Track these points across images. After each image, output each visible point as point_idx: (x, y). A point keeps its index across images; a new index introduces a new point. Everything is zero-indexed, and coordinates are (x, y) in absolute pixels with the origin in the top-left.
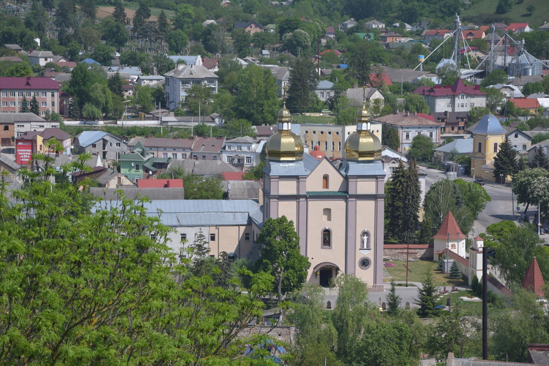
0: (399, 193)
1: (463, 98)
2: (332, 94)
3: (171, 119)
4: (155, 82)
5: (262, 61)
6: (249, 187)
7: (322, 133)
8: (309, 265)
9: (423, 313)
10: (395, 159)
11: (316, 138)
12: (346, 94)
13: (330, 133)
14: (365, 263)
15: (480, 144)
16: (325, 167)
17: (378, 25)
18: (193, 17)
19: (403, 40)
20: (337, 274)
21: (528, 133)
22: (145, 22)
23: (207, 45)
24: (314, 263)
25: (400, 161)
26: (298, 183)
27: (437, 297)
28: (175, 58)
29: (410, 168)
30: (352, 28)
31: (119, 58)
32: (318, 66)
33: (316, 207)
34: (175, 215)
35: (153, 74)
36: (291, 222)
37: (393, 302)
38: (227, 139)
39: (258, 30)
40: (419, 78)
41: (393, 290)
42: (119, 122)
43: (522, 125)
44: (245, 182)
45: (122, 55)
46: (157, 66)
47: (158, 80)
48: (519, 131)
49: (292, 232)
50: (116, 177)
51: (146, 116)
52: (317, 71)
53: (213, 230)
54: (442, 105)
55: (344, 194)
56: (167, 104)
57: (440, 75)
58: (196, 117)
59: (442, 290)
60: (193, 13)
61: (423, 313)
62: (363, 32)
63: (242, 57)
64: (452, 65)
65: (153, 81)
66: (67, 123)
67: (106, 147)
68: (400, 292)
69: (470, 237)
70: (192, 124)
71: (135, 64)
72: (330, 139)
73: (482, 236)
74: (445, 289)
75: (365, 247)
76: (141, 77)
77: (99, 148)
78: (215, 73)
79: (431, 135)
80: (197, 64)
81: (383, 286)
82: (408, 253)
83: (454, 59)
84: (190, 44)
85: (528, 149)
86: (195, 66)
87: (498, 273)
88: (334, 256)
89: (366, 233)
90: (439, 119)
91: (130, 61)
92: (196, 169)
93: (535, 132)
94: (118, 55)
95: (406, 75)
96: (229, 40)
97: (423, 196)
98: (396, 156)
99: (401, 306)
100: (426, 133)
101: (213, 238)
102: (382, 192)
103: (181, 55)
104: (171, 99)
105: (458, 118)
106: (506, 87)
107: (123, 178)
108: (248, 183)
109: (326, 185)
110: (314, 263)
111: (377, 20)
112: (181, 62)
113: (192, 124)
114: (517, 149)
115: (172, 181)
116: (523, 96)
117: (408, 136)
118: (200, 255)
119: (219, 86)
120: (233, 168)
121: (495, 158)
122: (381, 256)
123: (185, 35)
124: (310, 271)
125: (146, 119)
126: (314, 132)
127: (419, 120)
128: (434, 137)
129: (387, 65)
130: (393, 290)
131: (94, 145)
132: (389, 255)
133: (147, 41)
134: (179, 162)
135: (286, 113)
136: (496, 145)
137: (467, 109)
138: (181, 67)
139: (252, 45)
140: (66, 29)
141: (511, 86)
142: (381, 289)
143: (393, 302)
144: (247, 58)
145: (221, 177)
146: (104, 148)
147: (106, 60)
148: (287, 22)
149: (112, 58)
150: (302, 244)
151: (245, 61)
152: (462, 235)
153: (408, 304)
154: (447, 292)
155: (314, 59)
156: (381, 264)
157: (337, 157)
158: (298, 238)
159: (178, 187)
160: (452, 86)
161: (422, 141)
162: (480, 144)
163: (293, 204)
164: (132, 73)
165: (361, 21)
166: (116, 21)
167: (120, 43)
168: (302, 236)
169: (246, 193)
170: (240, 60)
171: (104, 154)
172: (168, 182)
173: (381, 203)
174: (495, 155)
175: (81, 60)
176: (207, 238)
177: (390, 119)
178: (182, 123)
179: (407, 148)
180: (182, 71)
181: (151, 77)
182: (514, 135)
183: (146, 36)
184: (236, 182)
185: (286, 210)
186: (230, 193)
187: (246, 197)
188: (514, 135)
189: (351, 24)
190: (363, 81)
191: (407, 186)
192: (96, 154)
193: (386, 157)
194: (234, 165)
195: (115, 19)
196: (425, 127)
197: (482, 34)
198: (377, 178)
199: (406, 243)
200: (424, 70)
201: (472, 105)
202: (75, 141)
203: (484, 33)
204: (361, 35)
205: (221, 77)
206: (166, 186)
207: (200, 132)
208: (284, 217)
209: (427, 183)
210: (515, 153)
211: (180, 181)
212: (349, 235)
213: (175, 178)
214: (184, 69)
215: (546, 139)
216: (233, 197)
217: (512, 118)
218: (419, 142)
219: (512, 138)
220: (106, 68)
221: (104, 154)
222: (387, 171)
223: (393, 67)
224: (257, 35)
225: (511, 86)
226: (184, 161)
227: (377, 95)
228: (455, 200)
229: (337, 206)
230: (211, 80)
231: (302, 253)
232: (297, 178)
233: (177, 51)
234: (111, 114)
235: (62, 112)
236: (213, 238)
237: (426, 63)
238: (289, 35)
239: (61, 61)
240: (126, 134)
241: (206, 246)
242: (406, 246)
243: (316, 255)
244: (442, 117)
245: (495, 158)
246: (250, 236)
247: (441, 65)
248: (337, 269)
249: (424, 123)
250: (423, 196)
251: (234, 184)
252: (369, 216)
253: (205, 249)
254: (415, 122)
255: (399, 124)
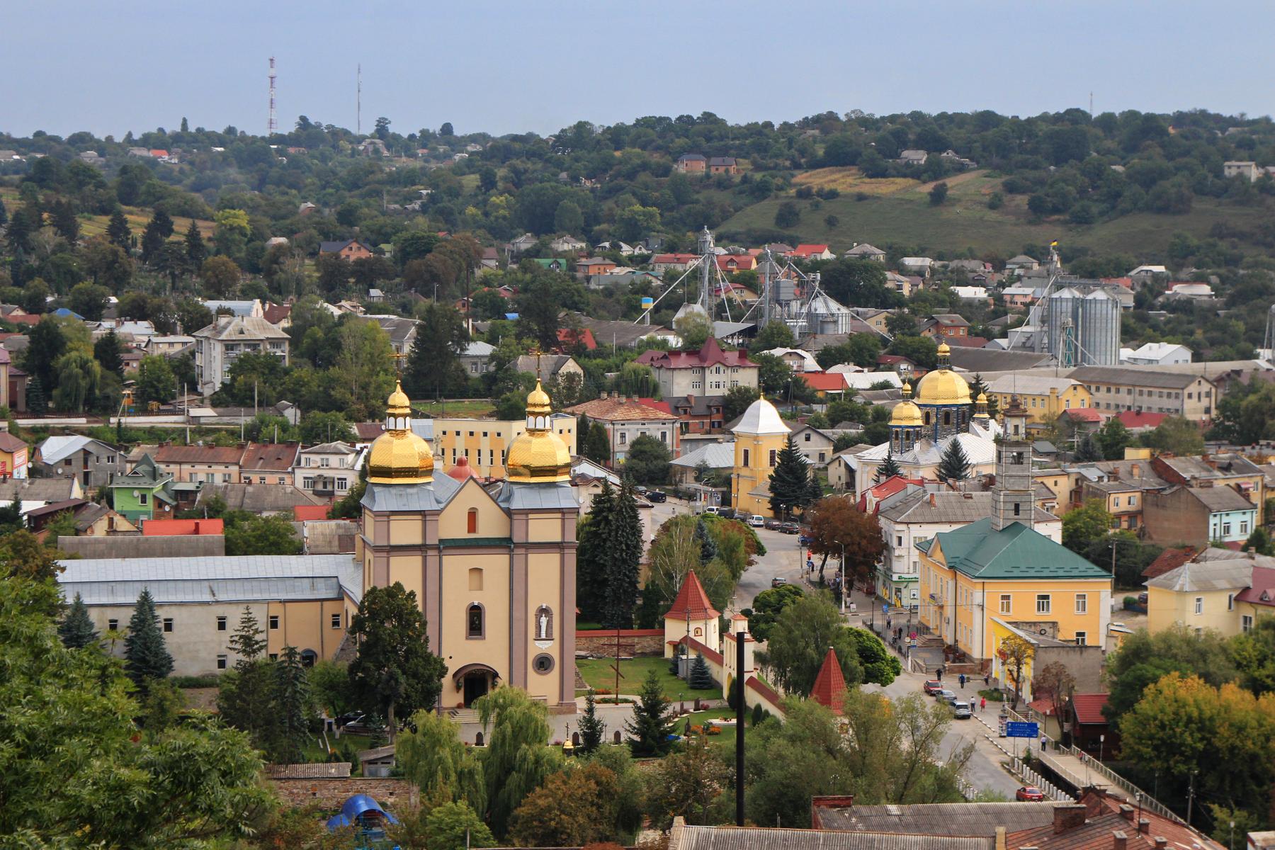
0: (605, 541)
1: (718, 371)
2: (492, 368)
3: (206, 413)
4: (178, 348)
5: (370, 309)
6: (341, 532)
7: (472, 434)
8: (443, 671)
9: (641, 750)
10: (598, 479)
11: (460, 444)
12: (516, 364)
13: (485, 434)
14: (543, 664)
15: (746, 452)
16: (474, 497)
17: (566, 245)
18: (249, 232)
19: (617, 270)
20: (494, 686)
21: (828, 432)
22: (162, 243)
23: (269, 282)
24: (453, 666)
25: (603, 481)
26: (424, 522)
27: (668, 719)
28: (213, 305)
29: (621, 496)
30: (527, 250)
31: (116, 305)
32: (467, 317)
33: (456, 566)
34: (206, 584)
35: (174, 333)
36: (412, 594)
37: (590, 736)
38: (303, 447)
39: (364, 254)
40: (644, 337)
41: (590, 711)
42: (113, 420)
43: (818, 419)
44: (333, 523)
45: (121, 302)
46: (182, 320)
47: (183, 343)
48: (816, 425)
49: (413, 610)
50: (106, 518)
51: (162, 407)
52: (465, 325)
53: (276, 610)
54: (681, 385)
55: (504, 544)
56: (199, 387)
57: (679, 333)
58: (250, 410)
59: (678, 708)
60: (248, 227)
61: (641, 750)
62: (546, 256)
63: (334, 301)
64: (699, 315)
65: (173, 345)
66: (22, 422)
67: (90, 464)
68: (601, 712)
69: (727, 615)
70: (244, 420)
71: (143, 318)
72: (485, 444)
73: (746, 613)
74: (682, 706)
75: (543, 636)
76: (154, 339)
77: (77, 467)
78: (284, 330)
79: (664, 434)
80: (254, 314)
81: (575, 704)
82: (619, 645)
83: (702, 304)
84: (244, 279)
85: (827, 460)
86: (250, 319)
87: (771, 676)
88: (490, 652)
89: (544, 611)
90: (677, 408)
91: (136, 312)
92: (247, 501)
93: (838, 432)
94: (114, 300)
95: (615, 332)
96: (308, 269)
97: (646, 547)
98: (600, 473)
99: (607, 737)
100: (654, 431)
101: (274, 624)
102: (571, 537)
103: (226, 299)
104: (206, 378)
105: (709, 407)
106: (790, 354)
107: (117, 519)
108: (338, 526)
109: (472, 527)
110: (453, 666)
111: (573, 236)
112: (229, 312)
113: (244, 420)
114: (809, 461)
115: (204, 524)
116: (820, 369)
117: (623, 436)
118: (248, 654)
119: (290, 352)
120: (315, 499)
121: (771, 477)
122: (572, 652)
123: (233, 265)
124: (447, 681)
125: (160, 413)
126: (458, 433)
127: (643, 411)
128: (668, 441)
129: (588, 315)
130: (590, 711)
131: (68, 462)
132: (587, 649)
133: (165, 276)
134: (218, 488)
135: (399, 398)
136: (773, 452)
137: (723, 392)
138: (223, 321)
139: (352, 280)
140: (25, 257)
141: (799, 351)
142: (571, 709)
143: (590, 736)
144: (343, 303)
145: (289, 512)
146: (86, 467)
147: (93, 311)
148: (415, 240)
149: (103, 307)
150: (431, 631)
151: (340, 307)
152: (711, 612)
153: (617, 735)
154: (686, 712)
155: (460, 304)
156: (571, 664)
157: (498, 477)
158: (424, 624)
159: (214, 530)
160: (698, 349)
161: (647, 448)
162: (746, 452)
163: (415, 561)
164: (138, 331)
165: (544, 237)
166: (112, 242)
167: (118, 281)
168: (431, 618)
169: (336, 543)
170: (330, 306)
171: (86, 475)
172: (197, 524)
173: (571, 558)
174: (771, 471)
175: (50, 311)
176: (262, 623)
177: (591, 409)
178: (226, 419)
179: (621, 458)
180: (225, 328)
181: (171, 338)
182: (803, 436)
183: (163, 268)
184: (318, 524)
185: (406, 573)
186: (307, 542)
187: (336, 549)
188: (803, 436)
189: (524, 242)
190: (548, 342)
191: (618, 527)
192: (71, 477)
193: (583, 476)
194: (316, 493)
195: (110, 239)
196: (652, 421)
197: (750, 263)
198: (563, 513)
199: (615, 628)
200: (653, 322)
201: (734, 382)
202: (34, 453)
203: (754, 261)
204: (544, 262)
205: (295, 335)
206: (197, 531)
207: (253, 434)
208: (398, 585)
209: (654, 521)
210: (804, 467)
211: (218, 523)
212: (515, 614)
213: (210, 517)
214: (229, 323)
215: (857, 443)
216: (313, 550)
217: (803, 406)
218: (642, 448)
219: (799, 440)
220: (91, 324)
221: (86, 475)
222: (584, 500)
223: (600, 318)
224: (360, 262)
225: (799, 351)
226: (226, 487)
227: (571, 366)
228: (699, 551)
229: (495, 563)
230: (275, 342)
231: (432, 647)
232: (422, 513)
233: (218, 294)
234: (98, 404)
235: (13, 404)
236: (274, 624)
237: (657, 309)
238: (415, 263)
239: (14, 313)
240: (125, 439)
241: (258, 637)
242: (615, 632)
243: (456, 651)
244: (682, 407)
245: (771, 477)
246: (342, 620)
247: (680, 314)
248: (495, 675)
249: (651, 416)
250: (646, 547)
251: (313, 528)
252: (549, 581)
253: (257, 643)
254: (636, 414)
255: (610, 417)
